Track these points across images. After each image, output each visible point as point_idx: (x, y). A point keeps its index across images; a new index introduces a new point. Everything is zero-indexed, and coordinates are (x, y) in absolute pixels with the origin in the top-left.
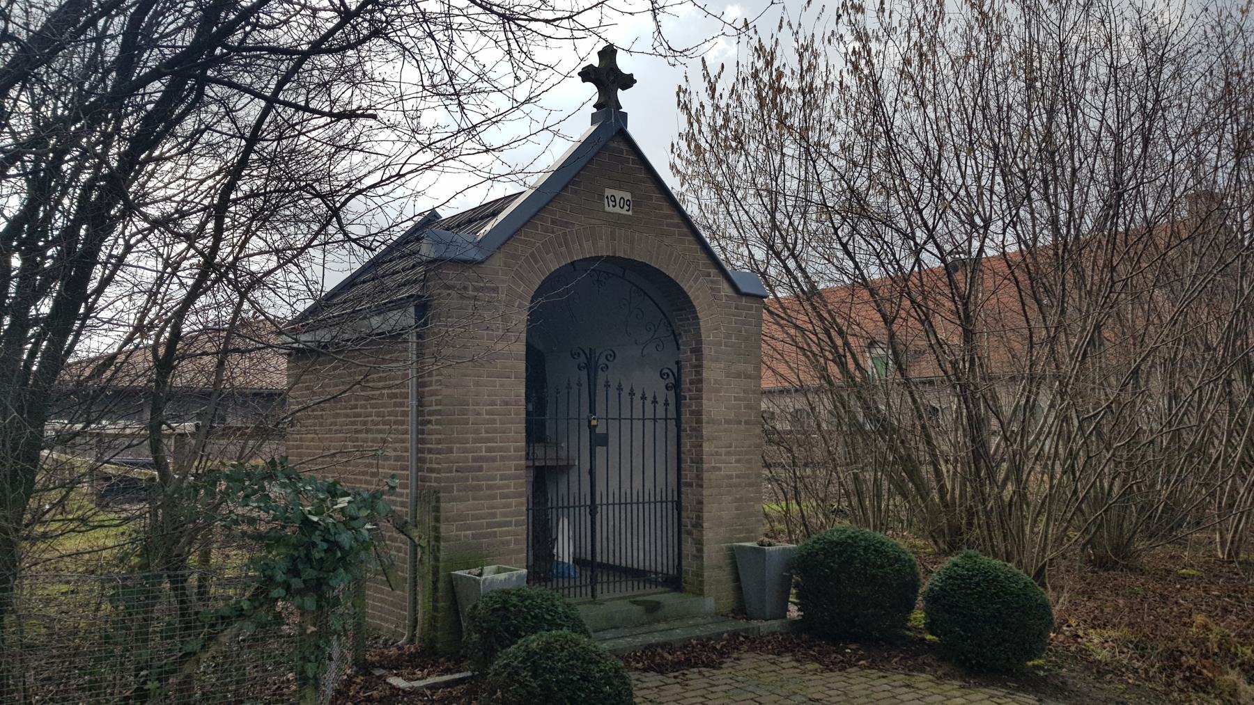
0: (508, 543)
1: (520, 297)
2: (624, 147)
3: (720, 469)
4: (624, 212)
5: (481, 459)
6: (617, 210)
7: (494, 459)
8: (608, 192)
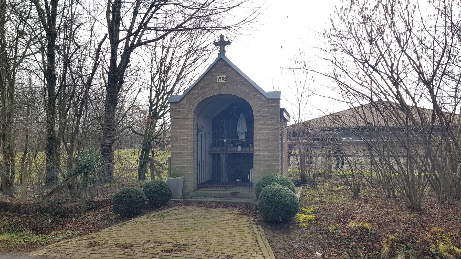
0: (188, 171)
1: (192, 109)
2: (223, 63)
3: (261, 155)
4: (224, 81)
5: (181, 150)
6: (222, 81)
7: (185, 151)
8: (218, 77)
